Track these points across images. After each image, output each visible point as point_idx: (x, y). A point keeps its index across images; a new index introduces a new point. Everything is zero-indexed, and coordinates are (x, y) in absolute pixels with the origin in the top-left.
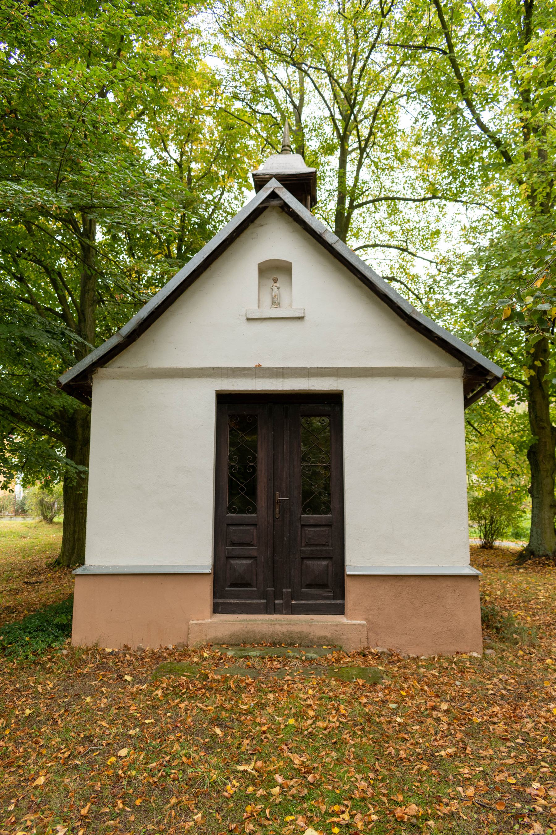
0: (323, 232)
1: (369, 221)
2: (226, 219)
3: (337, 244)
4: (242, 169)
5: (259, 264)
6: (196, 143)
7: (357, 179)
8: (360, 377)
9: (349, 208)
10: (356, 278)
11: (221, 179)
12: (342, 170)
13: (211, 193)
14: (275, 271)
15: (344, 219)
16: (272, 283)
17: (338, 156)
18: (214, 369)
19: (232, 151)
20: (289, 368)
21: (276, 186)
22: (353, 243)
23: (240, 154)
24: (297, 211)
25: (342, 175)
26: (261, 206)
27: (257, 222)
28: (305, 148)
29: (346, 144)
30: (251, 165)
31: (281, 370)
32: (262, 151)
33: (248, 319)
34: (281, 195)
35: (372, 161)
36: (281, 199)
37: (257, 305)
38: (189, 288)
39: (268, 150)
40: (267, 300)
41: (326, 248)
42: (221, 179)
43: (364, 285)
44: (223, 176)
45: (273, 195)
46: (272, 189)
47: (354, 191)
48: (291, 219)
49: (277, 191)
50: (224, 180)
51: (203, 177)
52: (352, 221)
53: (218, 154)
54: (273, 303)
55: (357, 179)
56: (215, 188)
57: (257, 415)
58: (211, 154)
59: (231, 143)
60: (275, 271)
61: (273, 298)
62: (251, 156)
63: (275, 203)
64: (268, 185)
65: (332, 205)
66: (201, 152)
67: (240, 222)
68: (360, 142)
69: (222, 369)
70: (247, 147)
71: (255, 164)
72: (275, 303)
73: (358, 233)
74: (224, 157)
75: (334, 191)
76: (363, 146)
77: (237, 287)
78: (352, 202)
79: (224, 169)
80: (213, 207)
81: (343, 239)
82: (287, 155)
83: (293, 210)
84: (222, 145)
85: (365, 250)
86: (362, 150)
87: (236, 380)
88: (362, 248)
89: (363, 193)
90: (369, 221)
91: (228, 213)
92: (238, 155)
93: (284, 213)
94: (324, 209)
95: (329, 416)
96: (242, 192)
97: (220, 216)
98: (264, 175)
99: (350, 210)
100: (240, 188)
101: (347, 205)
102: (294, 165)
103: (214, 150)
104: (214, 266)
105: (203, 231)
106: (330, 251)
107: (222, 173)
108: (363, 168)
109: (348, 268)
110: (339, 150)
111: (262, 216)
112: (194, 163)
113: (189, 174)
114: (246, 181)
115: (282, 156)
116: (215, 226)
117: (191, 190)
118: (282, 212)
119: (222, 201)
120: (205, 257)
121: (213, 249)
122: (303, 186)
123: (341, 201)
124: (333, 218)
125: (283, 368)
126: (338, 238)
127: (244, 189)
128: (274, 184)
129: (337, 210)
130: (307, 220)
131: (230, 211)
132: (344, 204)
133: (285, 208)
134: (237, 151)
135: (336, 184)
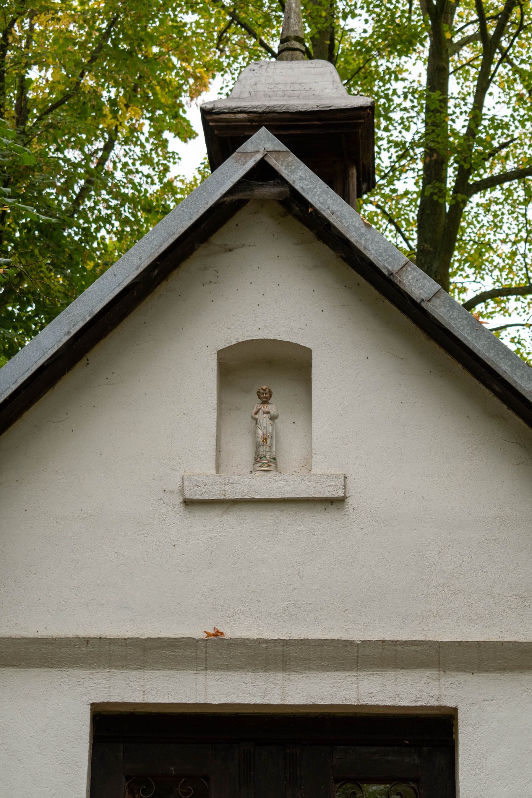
0: (396, 268)
1: (510, 226)
2: (119, 214)
3: (437, 302)
4: (165, 84)
5: (220, 353)
6: (43, 17)
7: (476, 115)
8: (504, 669)
9: (456, 190)
10: (487, 392)
11: (107, 110)
12: (436, 95)
13: (79, 145)
14: (264, 372)
15: (443, 221)
16: (257, 404)
17: (426, 54)
18: (87, 641)
19: (141, 40)
20: (301, 641)
21: (270, 146)
22: (468, 283)
23: (160, 45)
24: (326, 214)
25: (437, 105)
26: (228, 199)
27: (217, 239)
28: (338, 36)
29: (445, 27)
30: (187, 74)
31: (280, 648)
32: (220, 38)
33: (188, 503)
34: (284, 172)
35: (516, 70)
36: (283, 181)
37: (213, 463)
38: (26, 415)
39: (235, 38)
40: (241, 450)
41: (404, 311)
42: (107, 110)
43: (509, 413)
44: (113, 102)
45: (263, 172)
46: (259, 157)
47: (470, 147)
48: (309, 234)
49: (272, 161)
50: (114, 113)
51: (57, 104)
52: (463, 224)
53: (101, 47)
54: (258, 458)
55: (476, 115)
56: (92, 136)
57: (207, 779)
58: (83, 45)
59: (138, 19)
60: (264, 372)
61: (257, 446)
62: (190, 52)
63: (268, 191)
64: (248, 146)
65: (409, 183)
66: (56, 41)
67: (171, 241)
68: (482, 20)
69: (110, 641)
70: (180, 28)
71: (199, 72)
72: (265, 458)
73: (481, 255)
74: (117, 55)
75: (414, 144)
76: (491, 32)
77: (162, 413)
78: (463, 174)
79: (117, 85)
80: (82, 182)
81: (442, 279)
82: (295, 64)
83: (316, 211)
84: (113, 23)
85: (498, 303)
86: (490, 45)
87: (149, 673)
88: (494, 294)
89: (494, 152)
90: (510, 226)
91: (124, 199)
92: (155, 50)
93: (290, 217)
94: (387, 191)
95: (416, 781)
96: (164, 143)
97: (101, 206)
98: (232, 111)
99: (460, 197)
100: (157, 133)
101: (450, 183)
102: (317, 87)
103: (89, 34)
104: (96, 355)
105: (76, 264)
106: (415, 321)
107: (109, 93)
108: (493, 88)
109: (466, 366)
110: (428, 43)
111: (231, 223)
112: (35, 68)
113: (22, 96)
114: (176, 116)
115: (284, 64)
116: (86, 231)
117: (25, 137)
118: (284, 215)
119: (109, 165)
120: (73, 331)
121: (97, 310)
122: (338, 143)
123: (433, 172)
124: (413, 216)
125: (285, 643)
126: (440, 287)
127: (167, 135)
128: (263, 143)
129: (422, 194)
130: (352, 236)
131: (129, 191)
132: (443, 180)
133: (294, 205)
134: (152, 40)
135: (419, 126)
